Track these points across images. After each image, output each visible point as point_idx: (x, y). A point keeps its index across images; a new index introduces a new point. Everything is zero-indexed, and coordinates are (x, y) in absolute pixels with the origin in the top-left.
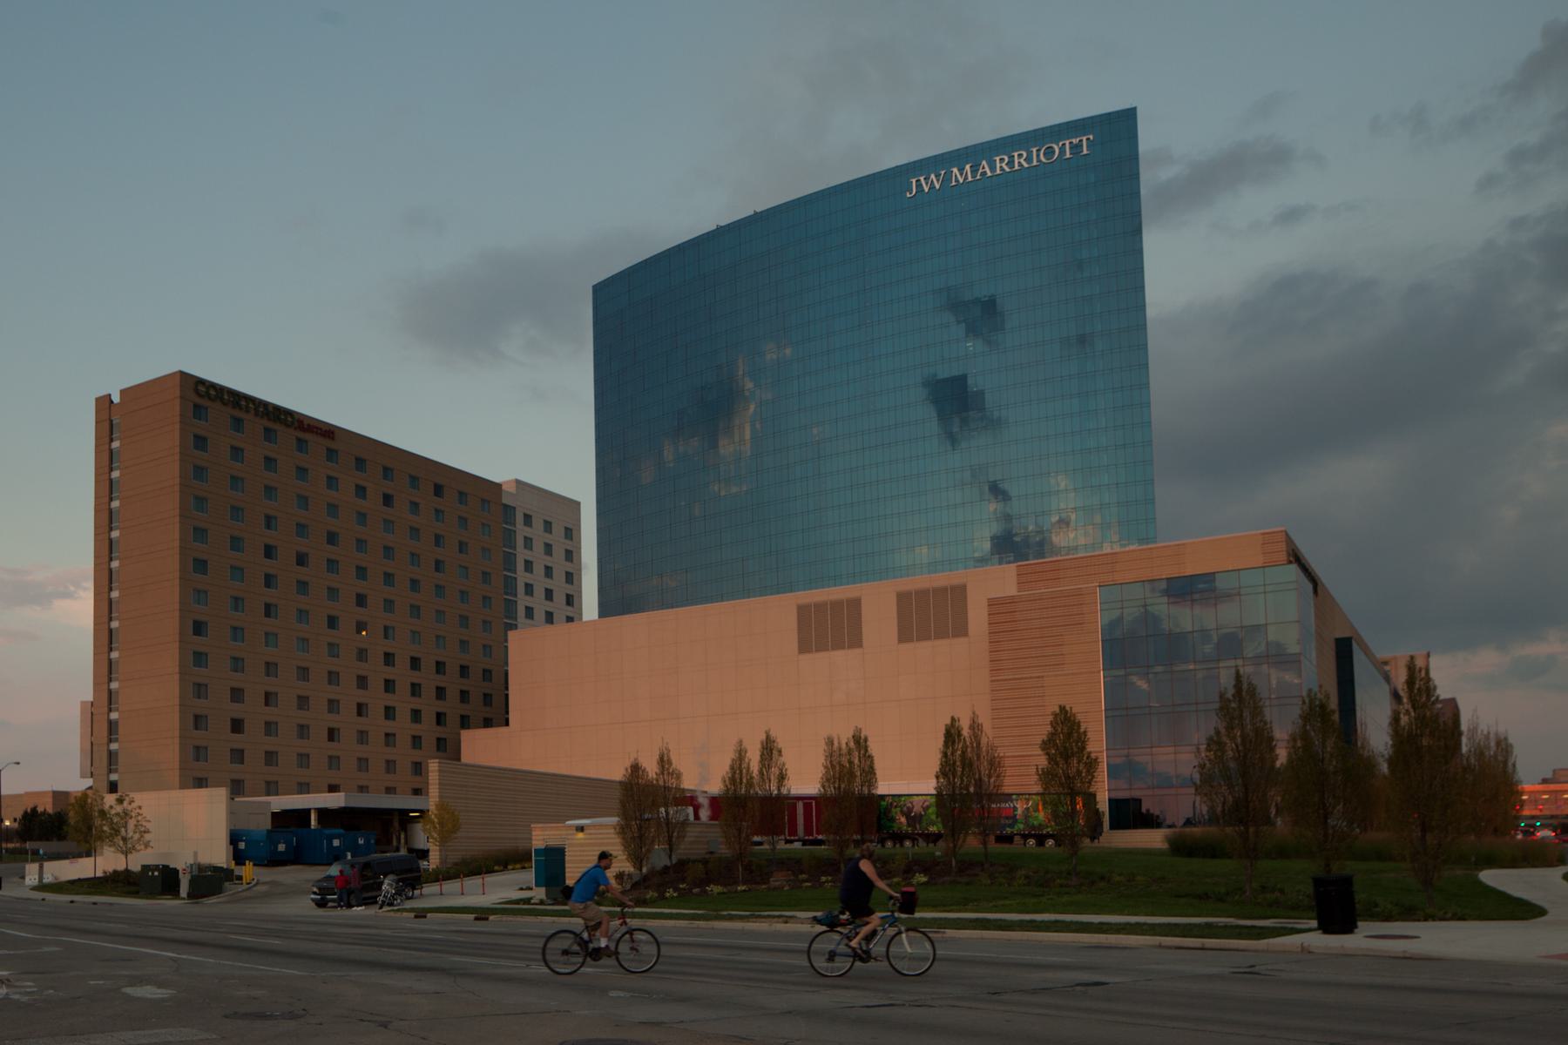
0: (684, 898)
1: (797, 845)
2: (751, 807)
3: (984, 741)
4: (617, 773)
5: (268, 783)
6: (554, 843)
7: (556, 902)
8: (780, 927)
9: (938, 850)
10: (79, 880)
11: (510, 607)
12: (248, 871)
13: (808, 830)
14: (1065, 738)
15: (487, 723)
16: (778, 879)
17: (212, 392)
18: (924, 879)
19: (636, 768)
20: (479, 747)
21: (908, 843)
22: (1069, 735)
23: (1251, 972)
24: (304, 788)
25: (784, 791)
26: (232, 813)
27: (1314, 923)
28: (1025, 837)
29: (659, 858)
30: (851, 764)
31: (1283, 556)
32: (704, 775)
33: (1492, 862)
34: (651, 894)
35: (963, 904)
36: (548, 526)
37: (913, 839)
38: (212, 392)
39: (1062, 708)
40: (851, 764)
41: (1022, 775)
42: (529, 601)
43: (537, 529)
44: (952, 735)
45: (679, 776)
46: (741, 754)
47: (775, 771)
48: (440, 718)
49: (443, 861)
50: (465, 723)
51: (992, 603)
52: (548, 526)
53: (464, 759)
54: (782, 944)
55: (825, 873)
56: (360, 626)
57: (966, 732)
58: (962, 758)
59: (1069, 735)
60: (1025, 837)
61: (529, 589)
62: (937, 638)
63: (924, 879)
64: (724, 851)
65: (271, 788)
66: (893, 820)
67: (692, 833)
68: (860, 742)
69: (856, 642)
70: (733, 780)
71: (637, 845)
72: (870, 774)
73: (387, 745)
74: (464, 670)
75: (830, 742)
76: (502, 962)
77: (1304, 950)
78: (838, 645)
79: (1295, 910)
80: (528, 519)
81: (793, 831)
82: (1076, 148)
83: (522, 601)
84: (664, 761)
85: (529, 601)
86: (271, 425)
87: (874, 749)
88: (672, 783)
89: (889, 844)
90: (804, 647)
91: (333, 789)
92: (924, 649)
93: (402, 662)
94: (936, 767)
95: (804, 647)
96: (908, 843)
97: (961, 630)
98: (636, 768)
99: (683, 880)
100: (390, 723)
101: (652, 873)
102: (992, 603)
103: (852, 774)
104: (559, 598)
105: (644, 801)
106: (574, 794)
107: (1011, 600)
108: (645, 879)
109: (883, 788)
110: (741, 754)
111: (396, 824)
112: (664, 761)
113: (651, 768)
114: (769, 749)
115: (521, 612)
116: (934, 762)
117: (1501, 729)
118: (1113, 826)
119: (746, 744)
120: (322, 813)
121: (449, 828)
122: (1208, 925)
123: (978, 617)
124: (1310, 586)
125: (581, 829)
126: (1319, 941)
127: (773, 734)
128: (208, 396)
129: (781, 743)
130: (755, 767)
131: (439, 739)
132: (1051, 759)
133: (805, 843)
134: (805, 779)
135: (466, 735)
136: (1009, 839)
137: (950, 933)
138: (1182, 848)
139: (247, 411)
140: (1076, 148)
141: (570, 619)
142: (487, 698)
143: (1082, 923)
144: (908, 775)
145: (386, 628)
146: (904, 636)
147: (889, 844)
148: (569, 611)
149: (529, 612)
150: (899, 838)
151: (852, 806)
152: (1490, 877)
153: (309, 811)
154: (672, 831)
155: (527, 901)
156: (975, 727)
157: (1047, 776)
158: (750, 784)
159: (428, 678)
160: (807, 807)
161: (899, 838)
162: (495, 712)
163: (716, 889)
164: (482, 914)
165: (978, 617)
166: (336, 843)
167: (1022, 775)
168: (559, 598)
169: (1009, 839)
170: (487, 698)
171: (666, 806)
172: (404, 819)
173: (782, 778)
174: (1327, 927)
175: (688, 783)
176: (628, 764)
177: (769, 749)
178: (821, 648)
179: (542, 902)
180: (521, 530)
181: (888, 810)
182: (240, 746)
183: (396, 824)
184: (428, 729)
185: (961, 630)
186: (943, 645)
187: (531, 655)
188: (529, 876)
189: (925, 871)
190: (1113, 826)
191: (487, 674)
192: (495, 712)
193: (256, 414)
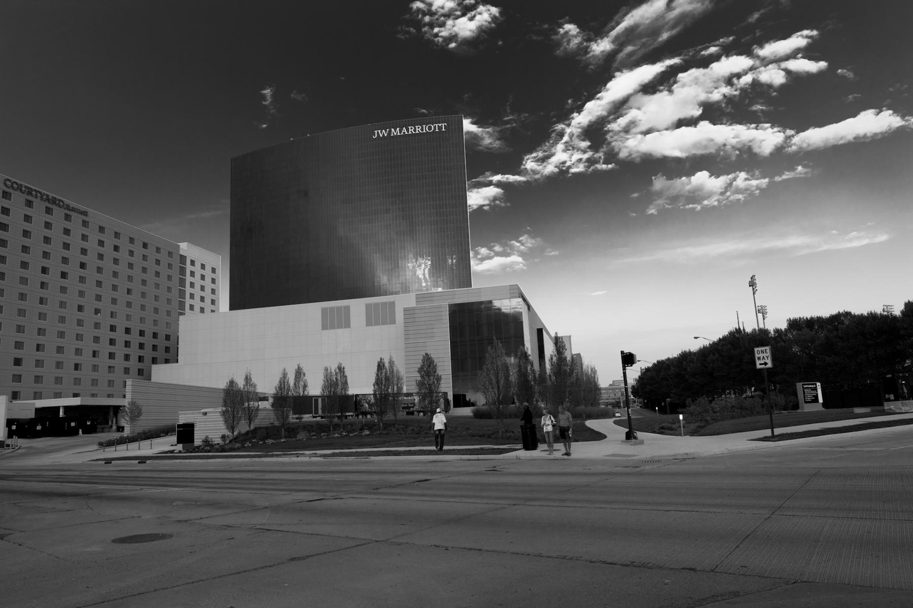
0: (254, 447)
1: (319, 419)
2: (290, 401)
3: (395, 369)
4: (222, 385)
5: (35, 393)
6: (190, 421)
7: (188, 451)
8: (294, 459)
9: (375, 418)
10: (718, 434)
11: (182, 305)
12: (16, 441)
13: (323, 411)
14: (428, 367)
15: (167, 361)
16: (302, 436)
17: (15, 186)
18: (367, 432)
19: (232, 382)
20: (161, 373)
21: (369, 416)
22: (429, 366)
23: (494, 470)
24: (58, 395)
25: (306, 393)
26: (8, 409)
27: (520, 446)
28: (419, 412)
29: (243, 427)
30: (336, 382)
31: (517, 295)
32: (267, 385)
33: (590, 417)
34: (237, 445)
35: (383, 444)
36: (203, 267)
37: (371, 414)
38: (15, 186)
39: (427, 354)
40: (336, 382)
41: (409, 384)
42: (192, 302)
43: (151, 252)
44: (381, 366)
45: (255, 386)
46: (285, 375)
47: (302, 383)
48: (141, 359)
49: (132, 432)
50: (154, 361)
51: (406, 310)
52: (203, 267)
53: (154, 379)
54: (304, 469)
55: (324, 432)
56: (97, 311)
57: (387, 365)
58: (385, 376)
59: (429, 366)
60: (419, 412)
61: (192, 296)
62: (383, 324)
63: (367, 432)
64: (277, 423)
65: (37, 396)
66: (362, 406)
67: (261, 415)
68: (341, 369)
69: (348, 325)
70: (280, 388)
71: (231, 420)
72: (345, 383)
73: (109, 372)
74: (142, 333)
75: (326, 369)
76: (129, 487)
77: (518, 458)
78: (340, 326)
79: (515, 441)
80: (193, 263)
81: (317, 412)
82: (440, 128)
83: (188, 302)
84: (248, 379)
85: (192, 302)
86: (50, 206)
87: (347, 373)
88: (251, 389)
89: (360, 417)
90: (324, 327)
91: (75, 395)
92: (376, 329)
93: (120, 330)
94: (373, 380)
95: (324, 327)
96: (369, 416)
97: (393, 321)
98: (232, 382)
99: (255, 438)
100: (127, 362)
101: (240, 434)
102: (406, 310)
103: (337, 384)
104: (208, 301)
105: (236, 399)
106: (195, 396)
107: (413, 309)
108: (235, 439)
109: (352, 391)
110: (285, 375)
111: (111, 414)
112: (248, 379)
113: (241, 383)
114: (299, 373)
115: (187, 307)
116: (373, 379)
117: (593, 364)
118: (454, 407)
119: (287, 371)
120: (67, 409)
121: (136, 412)
122: (482, 449)
123: (400, 316)
124: (526, 307)
125: (205, 414)
126: (523, 454)
127: (301, 366)
128: (13, 188)
129: (305, 370)
130: (292, 382)
131: (139, 370)
132: (422, 377)
133: (322, 417)
134: (315, 388)
135: (155, 367)
136: (412, 413)
137: (373, 458)
138: (478, 415)
139: (36, 197)
140: (440, 128)
141: (213, 311)
142: (167, 349)
143: (875, 423)
144: (361, 385)
145: (112, 313)
146: (369, 323)
147: (360, 417)
148: (213, 307)
149: (192, 307)
150: (365, 414)
151: (338, 400)
152: (591, 424)
153: (58, 408)
154: (251, 414)
155: (172, 452)
156: (391, 363)
157: (421, 384)
158: (289, 389)
159: (135, 339)
160: (323, 400)
161: (365, 414)
162: (170, 355)
163: (270, 441)
164: (142, 460)
165: (400, 316)
166: (73, 424)
167: (409, 384)
168: (208, 301)
169: (412, 413)
170: (167, 349)
171: (248, 401)
172: (117, 409)
173: (305, 386)
174: (527, 448)
175: (260, 389)
176: (228, 381)
177: (299, 373)
178: (332, 327)
179: (180, 452)
180: (189, 268)
181: (360, 401)
182: (19, 373)
183: (111, 414)
184: (134, 364)
185: (393, 321)
186: (385, 328)
187: (191, 329)
188: (174, 439)
189: (369, 429)
190: (454, 407)
191: (168, 337)
192: (170, 355)
193: (42, 199)
